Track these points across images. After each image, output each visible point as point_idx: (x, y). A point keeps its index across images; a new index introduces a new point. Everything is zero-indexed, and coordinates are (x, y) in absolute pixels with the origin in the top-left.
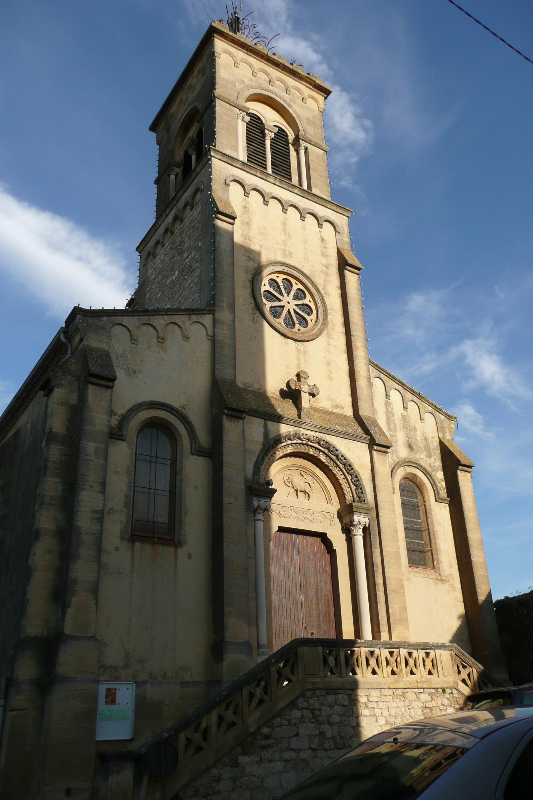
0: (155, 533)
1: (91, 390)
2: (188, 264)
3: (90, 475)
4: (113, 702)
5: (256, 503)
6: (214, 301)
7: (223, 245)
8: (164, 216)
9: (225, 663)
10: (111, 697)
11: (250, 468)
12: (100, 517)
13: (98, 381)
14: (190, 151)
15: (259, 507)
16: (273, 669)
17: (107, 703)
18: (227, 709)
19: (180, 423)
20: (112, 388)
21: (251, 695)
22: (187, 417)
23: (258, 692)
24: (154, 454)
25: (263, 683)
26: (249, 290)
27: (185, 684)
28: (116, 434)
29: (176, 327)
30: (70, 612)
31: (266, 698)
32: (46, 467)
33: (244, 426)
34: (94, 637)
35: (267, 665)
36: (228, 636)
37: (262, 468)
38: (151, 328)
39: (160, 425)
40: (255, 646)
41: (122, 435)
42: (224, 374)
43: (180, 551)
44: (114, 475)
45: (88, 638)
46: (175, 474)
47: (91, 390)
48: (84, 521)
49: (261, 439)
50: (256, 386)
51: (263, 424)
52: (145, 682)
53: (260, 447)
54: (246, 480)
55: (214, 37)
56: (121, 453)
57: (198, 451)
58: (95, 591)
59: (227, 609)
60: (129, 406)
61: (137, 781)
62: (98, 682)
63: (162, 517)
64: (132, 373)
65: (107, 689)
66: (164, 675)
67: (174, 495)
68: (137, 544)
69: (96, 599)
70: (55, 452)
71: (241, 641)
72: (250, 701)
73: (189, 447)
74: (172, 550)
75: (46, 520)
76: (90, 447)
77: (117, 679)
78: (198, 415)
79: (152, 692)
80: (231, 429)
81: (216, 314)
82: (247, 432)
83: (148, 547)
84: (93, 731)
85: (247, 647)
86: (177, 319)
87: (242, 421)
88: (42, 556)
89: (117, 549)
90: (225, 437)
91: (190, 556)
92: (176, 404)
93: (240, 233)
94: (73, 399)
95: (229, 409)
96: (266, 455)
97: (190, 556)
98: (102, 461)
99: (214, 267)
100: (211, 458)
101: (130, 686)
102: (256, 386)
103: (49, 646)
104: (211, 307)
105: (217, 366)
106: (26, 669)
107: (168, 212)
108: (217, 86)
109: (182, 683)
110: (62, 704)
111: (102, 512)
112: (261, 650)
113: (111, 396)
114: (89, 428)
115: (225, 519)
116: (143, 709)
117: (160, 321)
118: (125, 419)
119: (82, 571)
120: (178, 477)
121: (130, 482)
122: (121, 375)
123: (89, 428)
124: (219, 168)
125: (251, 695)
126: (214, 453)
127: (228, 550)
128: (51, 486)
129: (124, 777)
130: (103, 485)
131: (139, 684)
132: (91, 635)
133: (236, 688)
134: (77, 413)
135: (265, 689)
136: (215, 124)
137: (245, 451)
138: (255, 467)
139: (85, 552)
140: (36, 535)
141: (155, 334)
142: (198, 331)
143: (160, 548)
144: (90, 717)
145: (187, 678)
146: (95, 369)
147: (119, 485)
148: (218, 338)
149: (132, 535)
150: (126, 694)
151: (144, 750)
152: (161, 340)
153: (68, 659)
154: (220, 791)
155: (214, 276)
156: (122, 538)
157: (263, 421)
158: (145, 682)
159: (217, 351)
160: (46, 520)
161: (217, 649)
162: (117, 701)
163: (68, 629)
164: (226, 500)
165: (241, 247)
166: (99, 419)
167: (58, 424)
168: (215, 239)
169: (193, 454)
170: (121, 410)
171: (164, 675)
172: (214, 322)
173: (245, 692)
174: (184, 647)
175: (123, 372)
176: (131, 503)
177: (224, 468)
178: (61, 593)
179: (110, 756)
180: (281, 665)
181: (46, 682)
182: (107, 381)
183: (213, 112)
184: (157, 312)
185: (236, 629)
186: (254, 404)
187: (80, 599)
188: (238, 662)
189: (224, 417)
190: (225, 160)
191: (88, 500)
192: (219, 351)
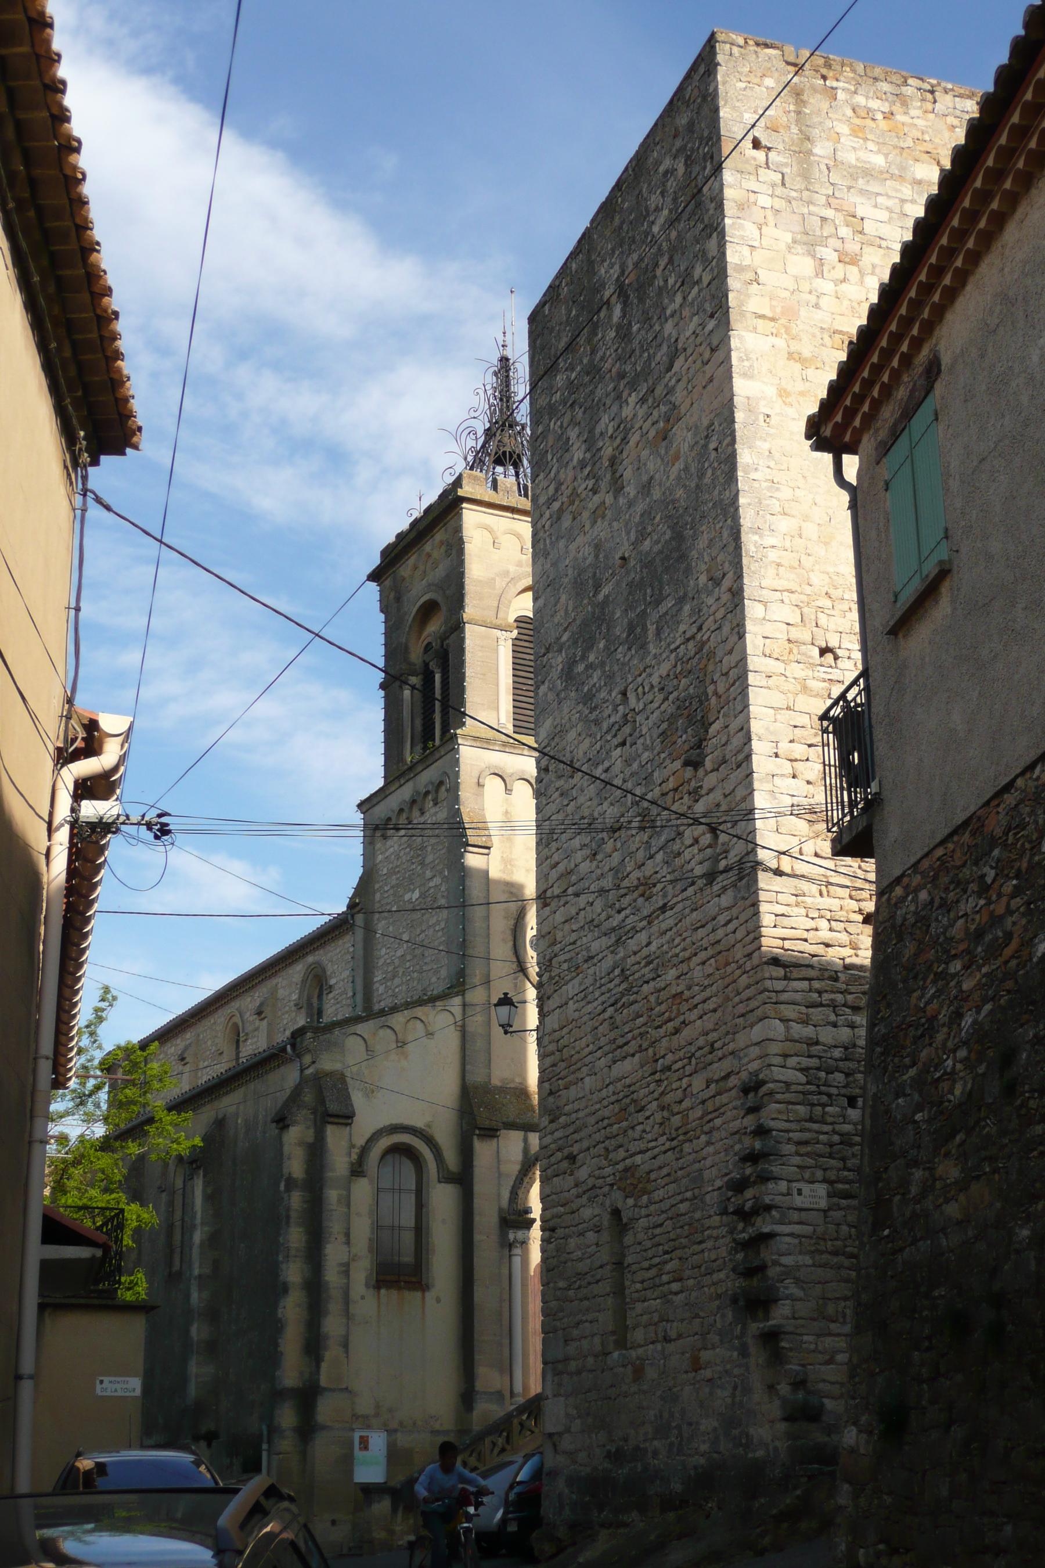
0: (400, 1273)
1: (330, 1131)
2: (432, 890)
3: (334, 1227)
4: (366, 1448)
5: (511, 1236)
6: (464, 978)
7: (475, 892)
8: (397, 785)
9: (475, 1413)
10: (364, 1444)
11: (506, 1194)
12: (346, 1270)
13: (336, 1120)
14: (432, 665)
15: (515, 1240)
16: (516, 1421)
17: (360, 1449)
18: (471, 1455)
19: (425, 1146)
20: (350, 1124)
21: (494, 1444)
22: (432, 1137)
23: (500, 1441)
24: (396, 1187)
25: (505, 1434)
26: (511, 944)
27: (435, 1433)
28: (357, 1170)
29: (418, 1022)
30: (324, 1365)
31: (508, 1447)
32: (288, 1217)
33: (767, 159)
34: (347, 1389)
35: (509, 1418)
36: (479, 1386)
37: (520, 1193)
38: (389, 1031)
39: (404, 1149)
40: (507, 1395)
41: (363, 1172)
42: (477, 1077)
43: (427, 1294)
44: (358, 1213)
45: (341, 1390)
46: (420, 1206)
47: (330, 1131)
48: (331, 1276)
49: (519, 1157)
50: (517, 1080)
51: (522, 1137)
52: (396, 1431)
53: (518, 1167)
54: (500, 1210)
55: (462, 508)
56: (362, 1190)
57: (447, 1178)
58: (345, 1345)
59: (477, 1357)
60: (367, 1135)
61: (395, 1509)
62: (353, 1430)
63: (408, 1258)
64: (370, 1092)
65: (361, 1437)
66: (415, 1424)
67: (420, 1230)
68: (383, 1291)
69: (347, 1352)
70: (296, 1200)
71: (491, 1390)
72: (492, 1450)
73: (436, 1174)
74: (419, 1294)
75: (293, 1273)
76: (332, 1195)
77: (369, 1427)
78: (445, 1136)
79: (403, 1440)
80: (483, 1150)
81: (467, 996)
82: (503, 1152)
83: (394, 1293)
84: (350, 1473)
85: (499, 1396)
86: (419, 1012)
87: (496, 1140)
88: (292, 1308)
89: (363, 1298)
90: (475, 1163)
91: (438, 1300)
92: (419, 1123)
93: (499, 858)
94: (310, 1136)
95: (480, 1129)
96: (525, 1175)
97: (438, 1300)
98: (346, 1210)
99: (464, 928)
100: (461, 1184)
101: (382, 1435)
102: (517, 1080)
103: (307, 1396)
104: (458, 985)
105: (468, 1067)
106: (287, 1417)
107: (402, 781)
108: (468, 600)
109: (432, 1432)
110: (323, 1449)
111: (347, 1265)
112: (513, 1400)
113: (350, 1134)
114: (330, 1174)
115: (475, 1260)
116: (395, 1456)
117: (398, 1020)
118: (365, 1150)
119: (332, 1325)
120: (424, 1210)
121: (372, 1224)
122: (358, 1099)
123: (330, 1174)
124: (471, 758)
125: (494, 1444)
126: (463, 1178)
127: (479, 1294)
128: (295, 1237)
129: (383, 1506)
130: (347, 1235)
131: (390, 1432)
132: (344, 1387)
133: (480, 1437)
134: (316, 1152)
135: (508, 1440)
136: (464, 673)
137: (500, 1175)
138: (511, 1193)
139: (334, 1307)
140: (285, 1289)
141: (394, 1038)
142: (443, 1020)
143: (407, 1294)
144: (347, 1461)
145: (437, 1427)
146: (333, 1107)
147: (362, 1229)
148: (470, 1028)
149: (377, 1281)
150: (378, 1441)
151: (399, 1486)
152: (401, 1044)
153: (325, 1409)
154: (341, 1265)
155: (464, 940)
156: (367, 1286)
157: (523, 1133)
158: (396, 1431)
159: (467, 1046)
160: (293, 1273)
161: (467, 1397)
162: (370, 1447)
163: (323, 1382)
164: (477, 1237)
165: (498, 882)
166: (339, 1161)
167: (296, 1166)
168: (463, 885)
169: (440, 1182)
170: (360, 1142)
171: (415, 1424)
172: (464, 1005)
173: (488, 1441)
174: (434, 1398)
175: (360, 1094)
176: (376, 1246)
177: (475, 1201)
178: (314, 1346)
179: (369, 1491)
180: (524, 1417)
181: (307, 1429)
182: (346, 1118)
183: (462, 640)
184: (394, 1009)
185: (487, 1378)
186: (511, 1113)
187: (332, 1353)
188: (487, 1411)
189: (475, 1137)
190: (478, 744)
191: (334, 1253)
192: (468, 1048)
